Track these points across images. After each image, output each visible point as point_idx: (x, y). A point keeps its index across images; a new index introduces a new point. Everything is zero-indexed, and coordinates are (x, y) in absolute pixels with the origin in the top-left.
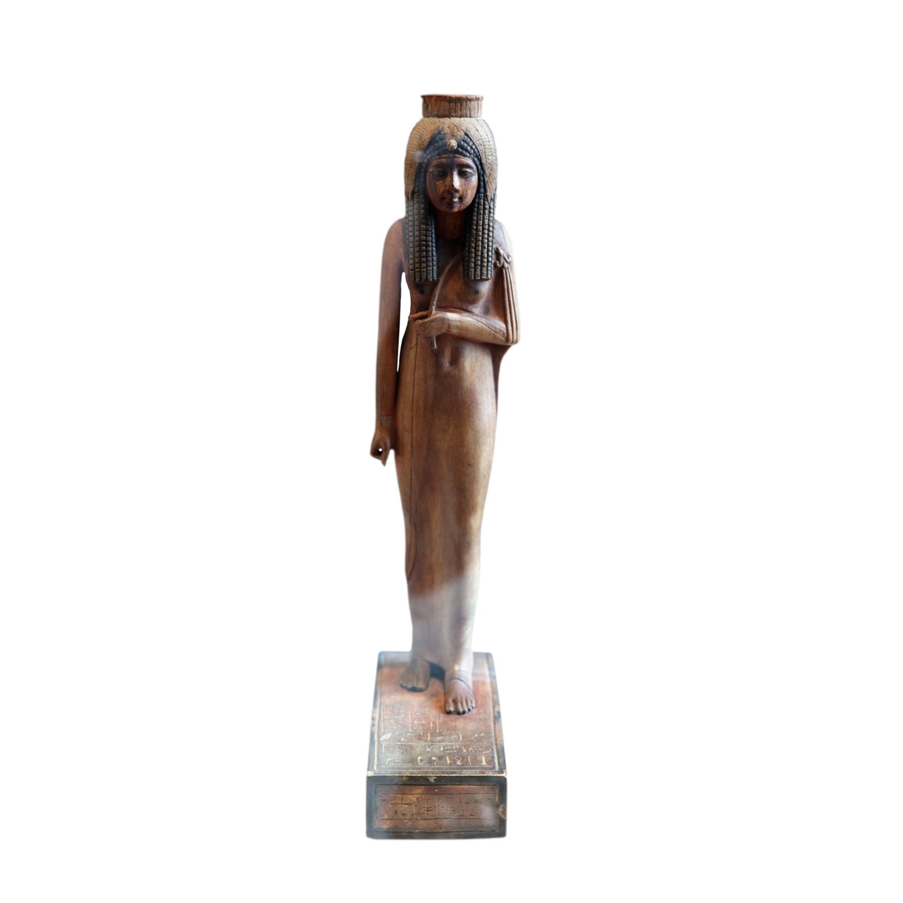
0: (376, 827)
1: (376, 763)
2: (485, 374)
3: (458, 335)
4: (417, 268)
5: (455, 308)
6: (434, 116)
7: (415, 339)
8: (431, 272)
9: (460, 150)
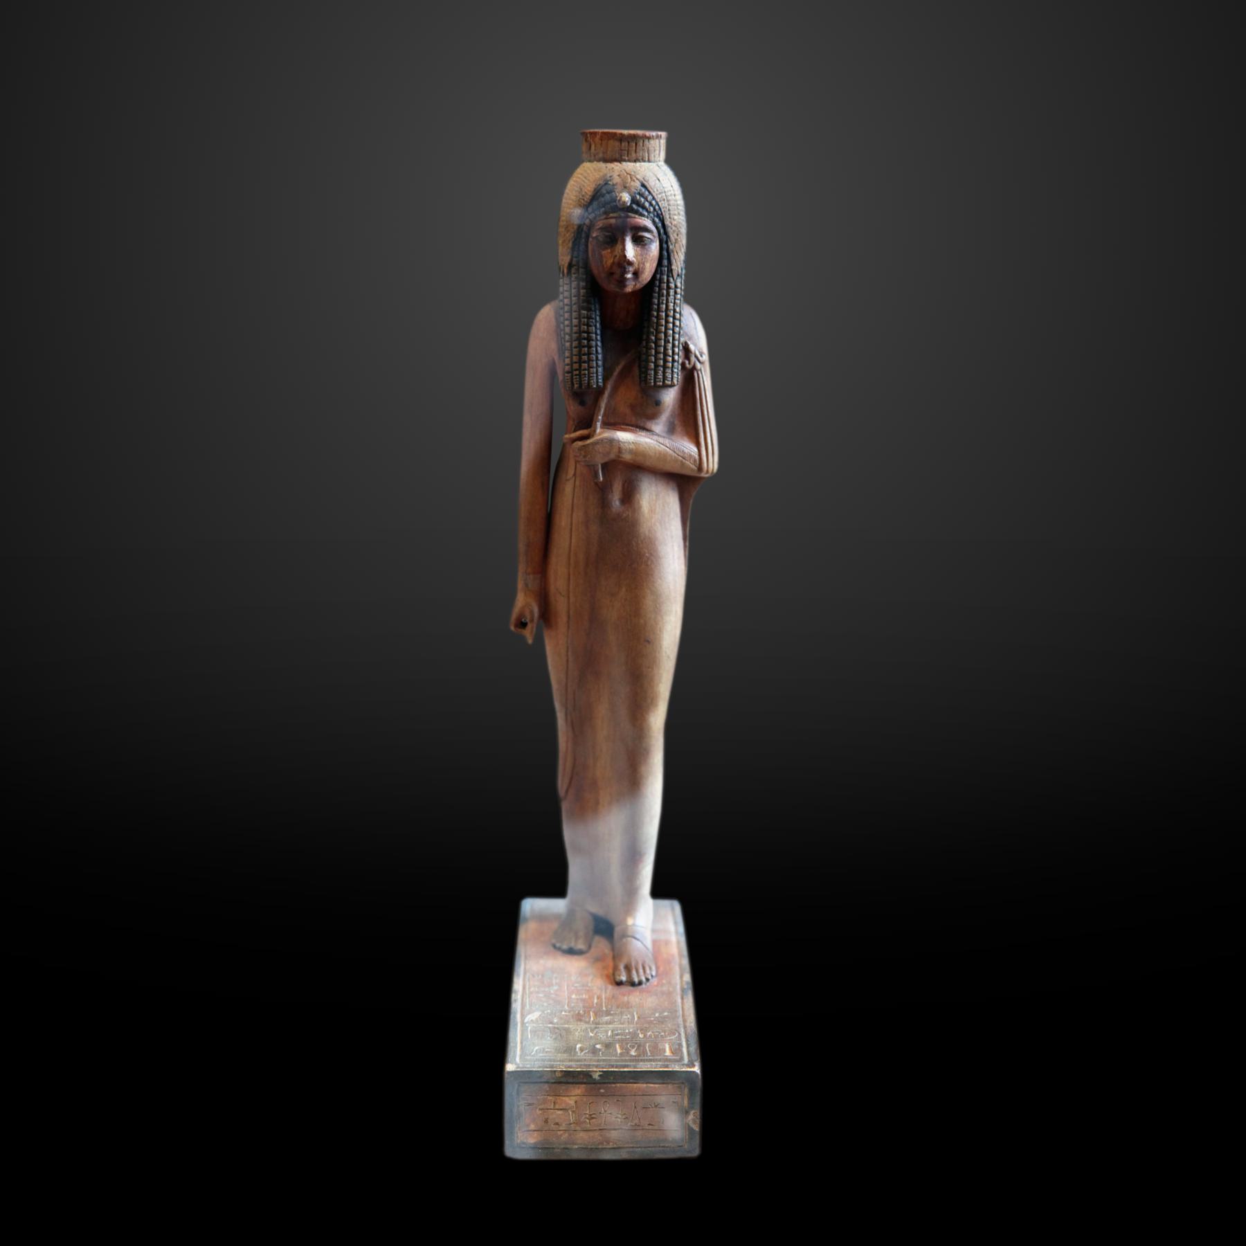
0: (519, 1141)
2: (669, 516)
3: (632, 462)
4: (576, 370)
5: (627, 425)
6: (599, 160)
7: (573, 467)
8: (595, 375)
9: (634, 206)
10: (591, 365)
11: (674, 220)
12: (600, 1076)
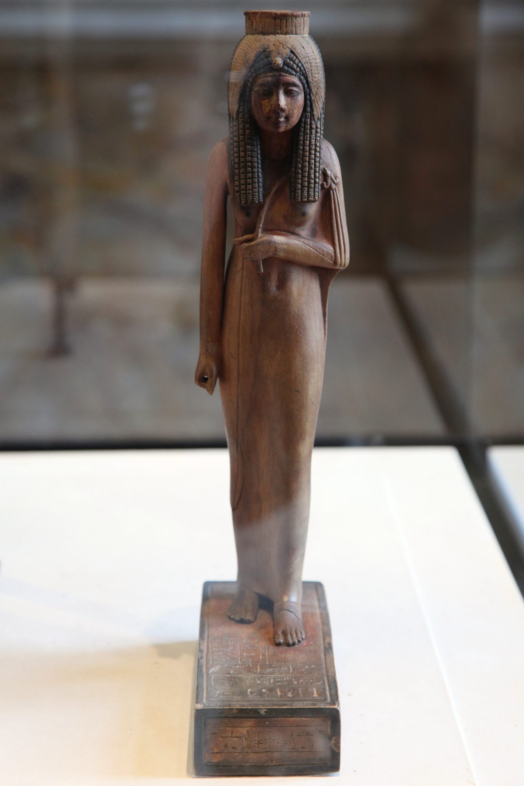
3: (284, 258)
4: (243, 190)
5: (281, 231)
6: (259, 34)
8: (257, 194)
9: (286, 68)
10: (254, 187)
11: (315, 77)
12: (265, 712)
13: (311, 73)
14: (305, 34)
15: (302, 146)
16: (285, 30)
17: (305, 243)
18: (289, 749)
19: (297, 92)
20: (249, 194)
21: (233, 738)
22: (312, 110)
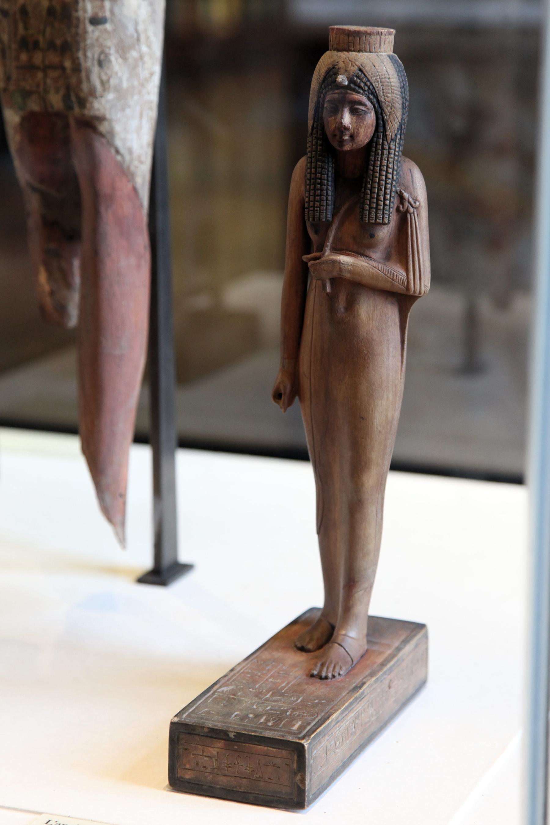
0: (179, 776)
1: (191, 710)
2: (386, 324)
4: (311, 207)
5: (350, 251)
6: (334, 50)
8: (325, 211)
9: (352, 85)
10: (322, 204)
11: (387, 97)
12: (234, 736)
13: (382, 92)
14: (383, 52)
15: (372, 166)
16: (358, 47)
17: (373, 266)
18: (257, 777)
19: (363, 111)
20: (316, 212)
21: (204, 757)
22: (385, 130)
